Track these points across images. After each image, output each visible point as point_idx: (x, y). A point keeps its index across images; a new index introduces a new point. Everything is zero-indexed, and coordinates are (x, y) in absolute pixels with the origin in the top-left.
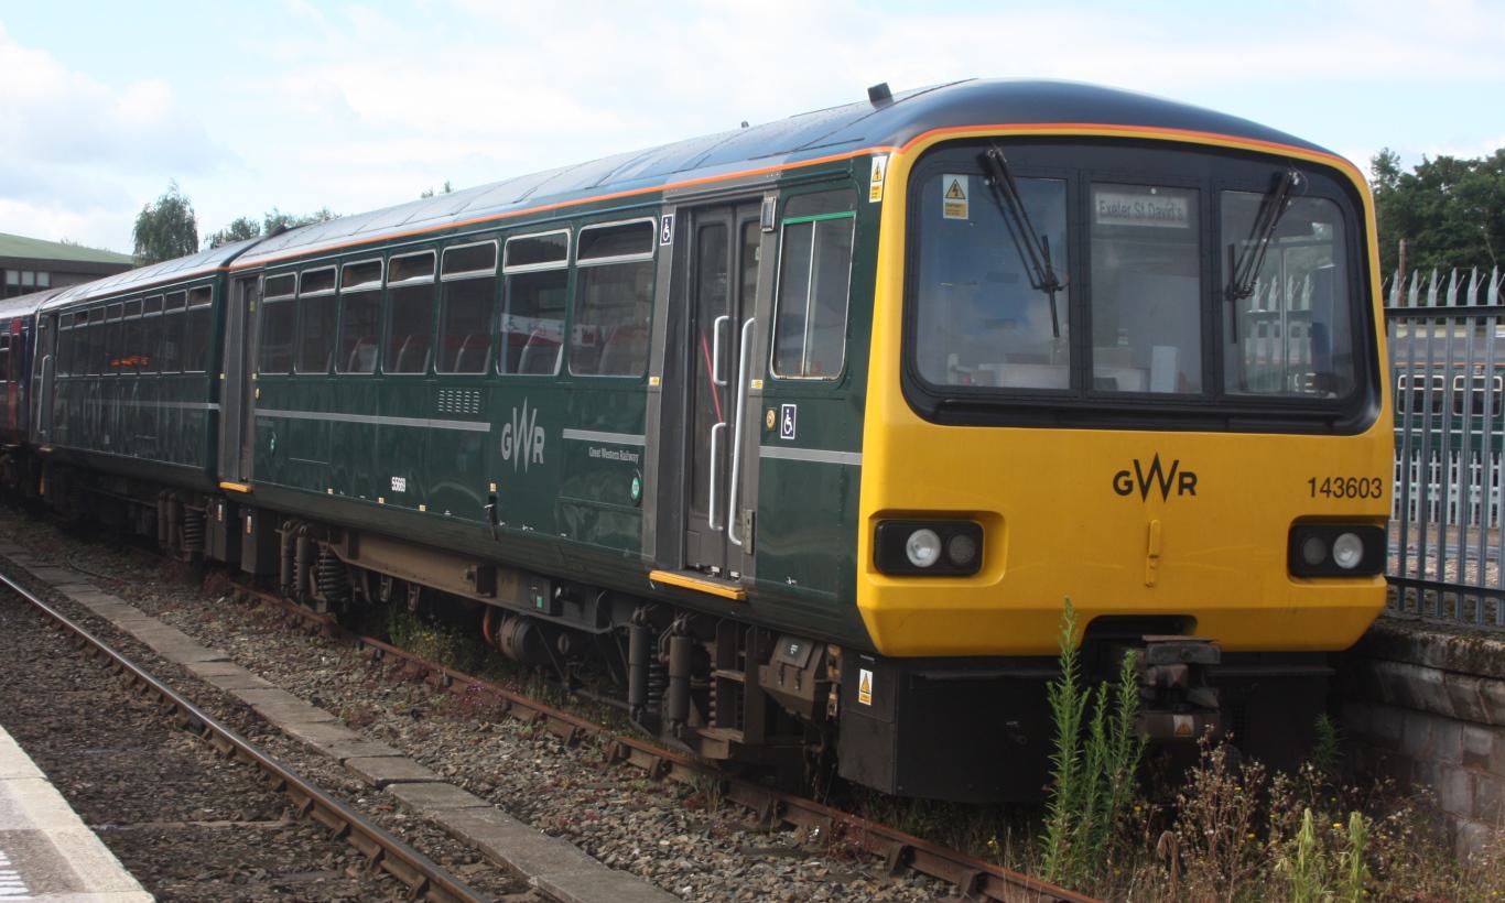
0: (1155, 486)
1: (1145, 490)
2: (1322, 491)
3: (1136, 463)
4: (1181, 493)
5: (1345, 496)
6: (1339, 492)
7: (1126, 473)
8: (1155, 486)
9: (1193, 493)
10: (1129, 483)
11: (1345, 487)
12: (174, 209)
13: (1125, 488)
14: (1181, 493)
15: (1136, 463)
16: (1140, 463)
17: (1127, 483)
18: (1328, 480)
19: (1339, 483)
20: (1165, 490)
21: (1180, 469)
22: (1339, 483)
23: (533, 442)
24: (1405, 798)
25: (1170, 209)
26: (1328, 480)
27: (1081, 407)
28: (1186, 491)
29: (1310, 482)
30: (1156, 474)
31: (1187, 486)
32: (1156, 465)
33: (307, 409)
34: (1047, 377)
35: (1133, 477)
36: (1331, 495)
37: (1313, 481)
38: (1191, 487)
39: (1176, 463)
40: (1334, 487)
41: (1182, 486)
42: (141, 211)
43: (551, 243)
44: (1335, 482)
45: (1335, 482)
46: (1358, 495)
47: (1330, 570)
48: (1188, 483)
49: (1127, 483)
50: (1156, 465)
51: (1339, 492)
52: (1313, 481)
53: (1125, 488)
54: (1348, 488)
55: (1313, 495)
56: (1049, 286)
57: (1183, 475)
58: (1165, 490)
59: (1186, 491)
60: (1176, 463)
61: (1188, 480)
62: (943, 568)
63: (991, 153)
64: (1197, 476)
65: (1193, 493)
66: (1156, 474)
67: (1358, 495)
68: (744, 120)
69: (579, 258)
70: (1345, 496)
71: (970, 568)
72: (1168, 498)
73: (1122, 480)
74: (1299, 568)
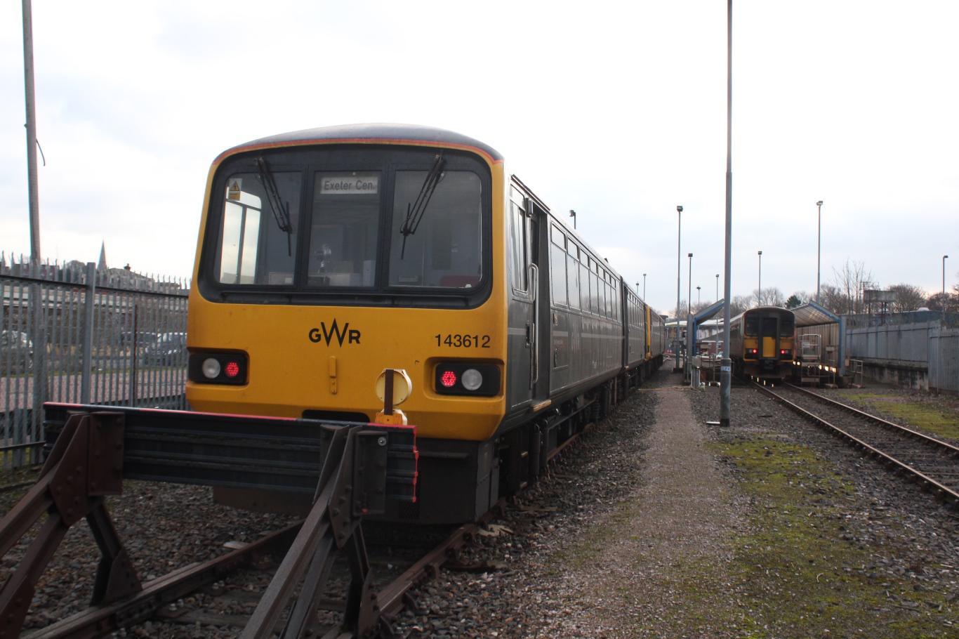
1: (328, 340)
2: (445, 342)
3: (323, 324)
4: (350, 342)
6: (458, 343)
7: (317, 330)
9: (358, 342)
10: (319, 336)
11: (462, 340)
14: (350, 342)
15: (323, 324)
17: (317, 335)
18: (450, 336)
19: (458, 338)
20: (341, 340)
21: (350, 328)
22: (458, 338)
25: (365, 186)
26: (450, 336)
27: (303, 292)
28: (354, 341)
31: (354, 338)
32: (335, 326)
34: (368, 279)
35: (321, 332)
36: (452, 345)
37: (439, 337)
38: (357, 339)
39: (347, 325)
40: (453, 340)
41: (351, 338)
43: (912, 291)
44: (455, 337)
45: (455, 337)
46: (462, 345)
47: (458, 390)
48: (355, 336)
49: (317, 335)
50: (335, 326)
51: (458, 343)
52: (439, 337)
54: (464, 341)
55: (439, 345)
56: (287, 229)
57: (351, 332)
58: (341, 340)
59: (354, 341)
60: (347, 325)
61: (354, 335)
62: (222, 380)
63: (274, 159)
64: (359, 330)
65: (358, 342)
66: (335, 330)
67: (462, 345)
71: (241, 379)
73: (314, 334)
74: (441, 390)
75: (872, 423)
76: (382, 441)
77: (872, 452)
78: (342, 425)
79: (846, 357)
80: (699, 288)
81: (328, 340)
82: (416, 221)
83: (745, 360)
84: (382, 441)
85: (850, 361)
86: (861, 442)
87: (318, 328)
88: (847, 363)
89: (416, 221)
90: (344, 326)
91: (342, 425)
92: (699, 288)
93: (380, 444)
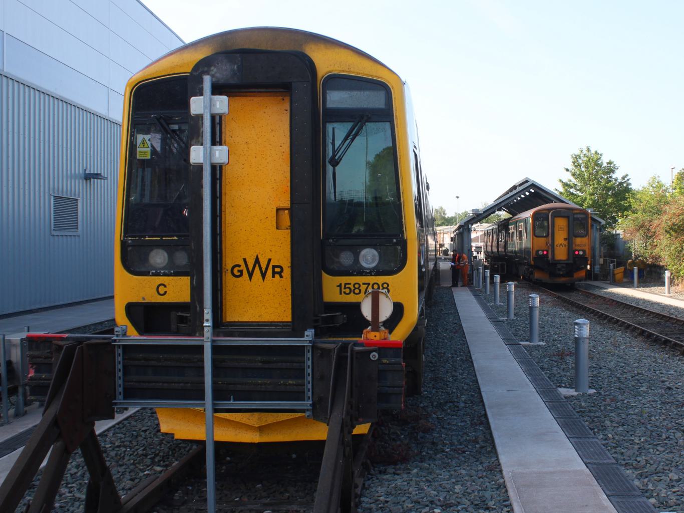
0: (561, 246)
1: (251, 275)
3: (245, 260)
4: (273, 277)
5: (352, 293)
7: (239, 266)
8: (561, 246)
9: (281, 277)
10: (241, 271)
12: (358, 119)
13: (239, 274)
14: (273, 277)
15: (245, 260)
16: (247, 260)
17: (239, 271)
20: (264, 275)
21: (272, 264)
23: (526, 230)
24: (619, 235)
28: (277, 276)
29: (337, 286)
30: (264, 270)
31: (277, 273)
32: (257, 261)
33: (214, 361)
35: (243, 267)
38: (280, 274)
39: (270, 260)
41: (274, 273)
42: (364, 164)
49: (239, 271)
50: (257, 261)
53: (239, 274)
57: (274, 267)
58: (264, 275)
59: (277, 276)
60: (270, 260)
61: (277, 270)
65: (281, 277)
66: (264, 270)
68: (459, 196)
69: (322, 443)
70: (352, 293)
72: (253, 278)
75: (643, 313)
76: (374, 356)
77: (663, 339)
78: (334, 343)
79: (601, 257)
80: (458, 197)
81: (251, 275)
82: (112, 214)
83: (505, 263)
84: (374, 356)
85: (604, 260)
86: (643, 328)
87: (240, 264)
88: (601, 261)
89: (112, 214)
90: (267, 262)
91: (334, 343)
92: (458, 197)
93: (373, 359)
